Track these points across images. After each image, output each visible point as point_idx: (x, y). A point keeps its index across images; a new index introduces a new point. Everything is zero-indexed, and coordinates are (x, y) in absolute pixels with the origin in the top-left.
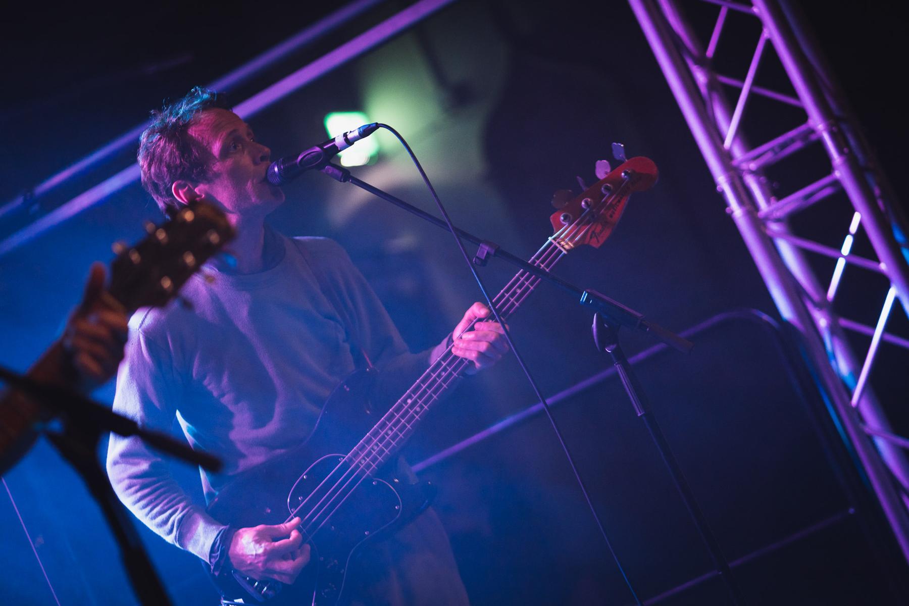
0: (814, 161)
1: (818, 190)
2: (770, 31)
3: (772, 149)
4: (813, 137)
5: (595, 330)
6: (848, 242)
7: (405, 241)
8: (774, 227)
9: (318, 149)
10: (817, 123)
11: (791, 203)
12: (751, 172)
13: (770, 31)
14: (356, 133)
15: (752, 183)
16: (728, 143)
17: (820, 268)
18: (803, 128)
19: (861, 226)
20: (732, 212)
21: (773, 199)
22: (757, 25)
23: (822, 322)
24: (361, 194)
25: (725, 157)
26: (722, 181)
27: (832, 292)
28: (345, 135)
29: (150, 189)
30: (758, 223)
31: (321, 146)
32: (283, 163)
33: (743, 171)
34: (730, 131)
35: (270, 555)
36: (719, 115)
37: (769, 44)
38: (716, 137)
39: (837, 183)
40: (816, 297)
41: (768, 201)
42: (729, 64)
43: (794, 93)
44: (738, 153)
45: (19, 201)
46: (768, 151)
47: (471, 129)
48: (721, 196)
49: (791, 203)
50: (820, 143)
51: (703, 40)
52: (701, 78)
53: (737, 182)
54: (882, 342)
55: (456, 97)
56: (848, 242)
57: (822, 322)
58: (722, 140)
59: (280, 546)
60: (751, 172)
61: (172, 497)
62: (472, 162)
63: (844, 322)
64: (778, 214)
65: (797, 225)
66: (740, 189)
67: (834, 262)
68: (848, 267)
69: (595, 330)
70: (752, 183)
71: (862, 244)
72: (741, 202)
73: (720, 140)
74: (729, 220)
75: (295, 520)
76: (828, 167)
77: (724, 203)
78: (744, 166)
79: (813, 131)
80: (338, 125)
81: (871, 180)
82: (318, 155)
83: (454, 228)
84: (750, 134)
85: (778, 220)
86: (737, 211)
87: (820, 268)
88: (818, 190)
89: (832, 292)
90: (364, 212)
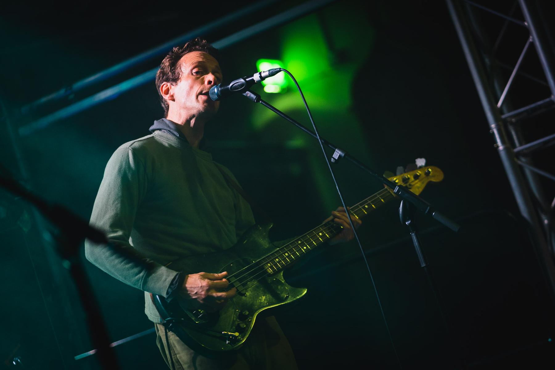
2: (534, 38)
5: (401, 210)
7: (297, 142)
9: (242, 80)
14: (267, 73)
22: (527, 32)
24: (270, 114)
28: (174, 94)
30: (513, 156)
31: (245, 79)
32: (221, 87)
35: (210, 288)
37: (532, 45)
45: (62, 92)
47: (344, 81)
52: (487, 61)
53: (503, 129)
55: (339, 58)
59: (217, 283)
60: (512, 123)
62: (343, 99)
69: (401, 210)
75: (225, 273)
77: (495, 142)
80: (264, 66)
82: (242, 85)
90: (272, 125)
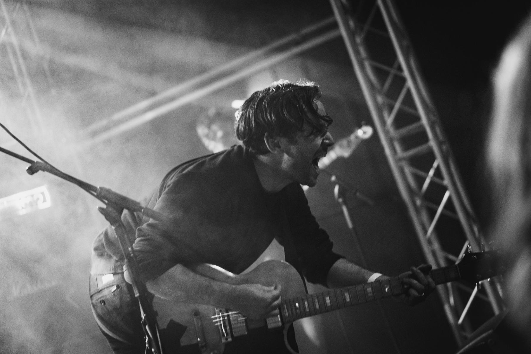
0: (422, 137)
2: (410, 83)
6: (431, 173)
11: (411, 153)
13: (410, 83)
17: (420, 181)
19: (450, 199)
22: (403, 80)
25: (387, 133)
27: (460, 321)
29: (111, 254)
34: (389, 120)
36: (386, 114)
42: (392, 94)
43: (415, 108)
44: (392, 130)
46: (405, 130)
49: (411, 153)
54: (442, 215)
56: (431, 173)
61: (172, 176)
71: (438, 170)
89: (460, 321)
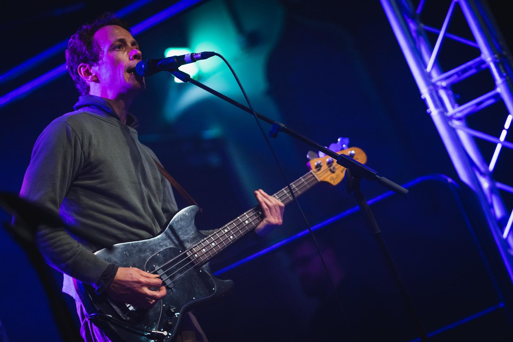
1: (485, 99)
3: (457, 73)
4: (483, 66)
6: (504, 133)
8: (456, 123)
10: (486, 56)
11: (468, 106)
12: (444, 88)
15: (443, 94)
16: (429, 69)
18: (478, 59)
20: (431, 112)
21: (456, 105)
23: (485, 184)
25: (427, 77)
26: (425, 93)
30: (447, 119)
33: (438, 86)
34: (430, 62)
38: (422, 64)
39: (498, 95)
40: (482, 169)
41: (453, 107)
43: (474, 40)
44: (435, 77)
48: (424, 101)
49: (468, 106)
50: (489, 68)
51: (487, 161)
54: (440, 29)
56: (504, 133)
57: (485, 184)
58: (426, 67)
60: (444, 88)
63: (499, 185)
64: (459, 115)
65: (470, 121)
66: (436, 98)
67: (495, 145)
68: (503, 148)
70: (443, 94)
72: (436, 106)
73: (426, 74)
74: (429, 116)
76: (494, 86)
77: (427, 107)
78: (439, 84)
79: (483, 62)
81: (501, 67)
83: (254, 115)
84: (442, 64)
85: (459, 119)
86: (434, 112)
87: (485, 149)
88: (485, 99)
89: (492, 166)
